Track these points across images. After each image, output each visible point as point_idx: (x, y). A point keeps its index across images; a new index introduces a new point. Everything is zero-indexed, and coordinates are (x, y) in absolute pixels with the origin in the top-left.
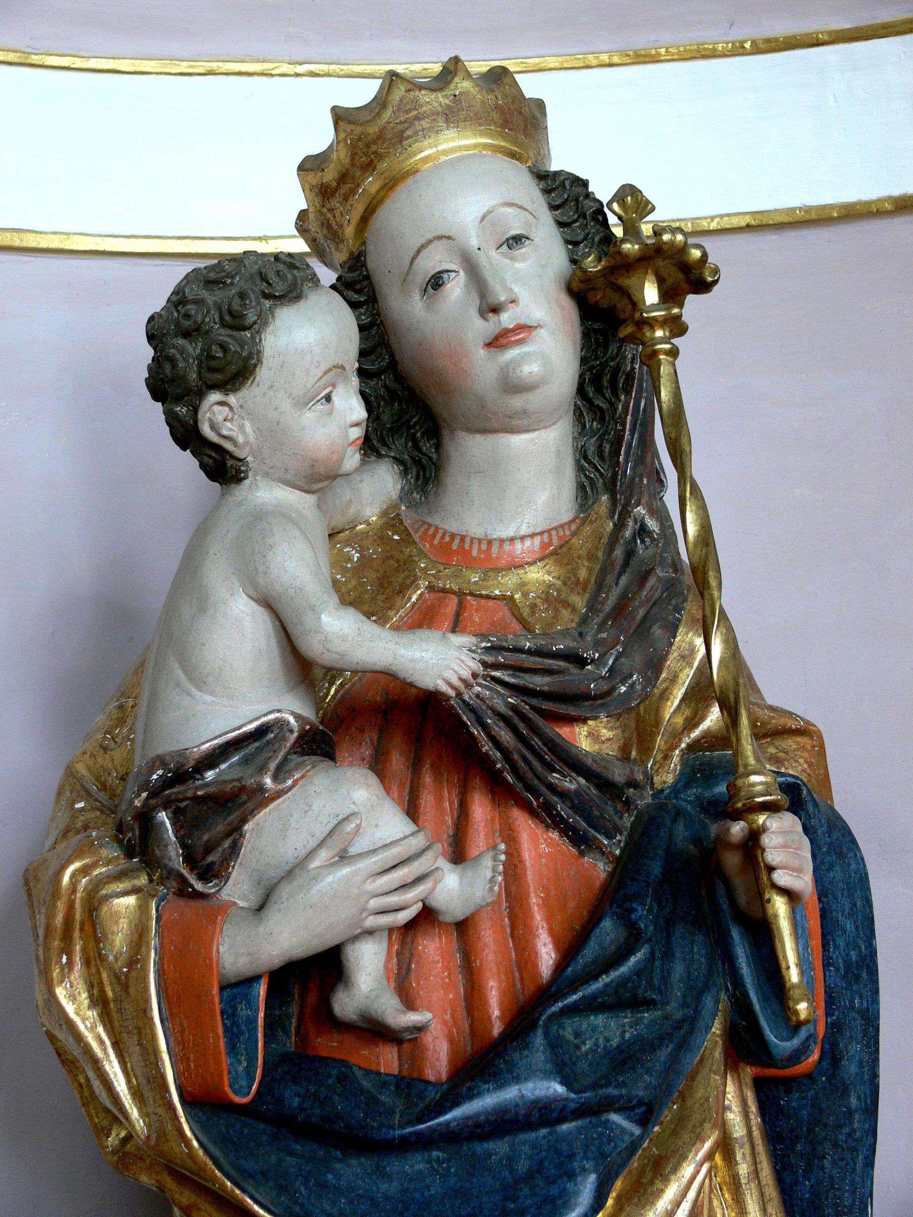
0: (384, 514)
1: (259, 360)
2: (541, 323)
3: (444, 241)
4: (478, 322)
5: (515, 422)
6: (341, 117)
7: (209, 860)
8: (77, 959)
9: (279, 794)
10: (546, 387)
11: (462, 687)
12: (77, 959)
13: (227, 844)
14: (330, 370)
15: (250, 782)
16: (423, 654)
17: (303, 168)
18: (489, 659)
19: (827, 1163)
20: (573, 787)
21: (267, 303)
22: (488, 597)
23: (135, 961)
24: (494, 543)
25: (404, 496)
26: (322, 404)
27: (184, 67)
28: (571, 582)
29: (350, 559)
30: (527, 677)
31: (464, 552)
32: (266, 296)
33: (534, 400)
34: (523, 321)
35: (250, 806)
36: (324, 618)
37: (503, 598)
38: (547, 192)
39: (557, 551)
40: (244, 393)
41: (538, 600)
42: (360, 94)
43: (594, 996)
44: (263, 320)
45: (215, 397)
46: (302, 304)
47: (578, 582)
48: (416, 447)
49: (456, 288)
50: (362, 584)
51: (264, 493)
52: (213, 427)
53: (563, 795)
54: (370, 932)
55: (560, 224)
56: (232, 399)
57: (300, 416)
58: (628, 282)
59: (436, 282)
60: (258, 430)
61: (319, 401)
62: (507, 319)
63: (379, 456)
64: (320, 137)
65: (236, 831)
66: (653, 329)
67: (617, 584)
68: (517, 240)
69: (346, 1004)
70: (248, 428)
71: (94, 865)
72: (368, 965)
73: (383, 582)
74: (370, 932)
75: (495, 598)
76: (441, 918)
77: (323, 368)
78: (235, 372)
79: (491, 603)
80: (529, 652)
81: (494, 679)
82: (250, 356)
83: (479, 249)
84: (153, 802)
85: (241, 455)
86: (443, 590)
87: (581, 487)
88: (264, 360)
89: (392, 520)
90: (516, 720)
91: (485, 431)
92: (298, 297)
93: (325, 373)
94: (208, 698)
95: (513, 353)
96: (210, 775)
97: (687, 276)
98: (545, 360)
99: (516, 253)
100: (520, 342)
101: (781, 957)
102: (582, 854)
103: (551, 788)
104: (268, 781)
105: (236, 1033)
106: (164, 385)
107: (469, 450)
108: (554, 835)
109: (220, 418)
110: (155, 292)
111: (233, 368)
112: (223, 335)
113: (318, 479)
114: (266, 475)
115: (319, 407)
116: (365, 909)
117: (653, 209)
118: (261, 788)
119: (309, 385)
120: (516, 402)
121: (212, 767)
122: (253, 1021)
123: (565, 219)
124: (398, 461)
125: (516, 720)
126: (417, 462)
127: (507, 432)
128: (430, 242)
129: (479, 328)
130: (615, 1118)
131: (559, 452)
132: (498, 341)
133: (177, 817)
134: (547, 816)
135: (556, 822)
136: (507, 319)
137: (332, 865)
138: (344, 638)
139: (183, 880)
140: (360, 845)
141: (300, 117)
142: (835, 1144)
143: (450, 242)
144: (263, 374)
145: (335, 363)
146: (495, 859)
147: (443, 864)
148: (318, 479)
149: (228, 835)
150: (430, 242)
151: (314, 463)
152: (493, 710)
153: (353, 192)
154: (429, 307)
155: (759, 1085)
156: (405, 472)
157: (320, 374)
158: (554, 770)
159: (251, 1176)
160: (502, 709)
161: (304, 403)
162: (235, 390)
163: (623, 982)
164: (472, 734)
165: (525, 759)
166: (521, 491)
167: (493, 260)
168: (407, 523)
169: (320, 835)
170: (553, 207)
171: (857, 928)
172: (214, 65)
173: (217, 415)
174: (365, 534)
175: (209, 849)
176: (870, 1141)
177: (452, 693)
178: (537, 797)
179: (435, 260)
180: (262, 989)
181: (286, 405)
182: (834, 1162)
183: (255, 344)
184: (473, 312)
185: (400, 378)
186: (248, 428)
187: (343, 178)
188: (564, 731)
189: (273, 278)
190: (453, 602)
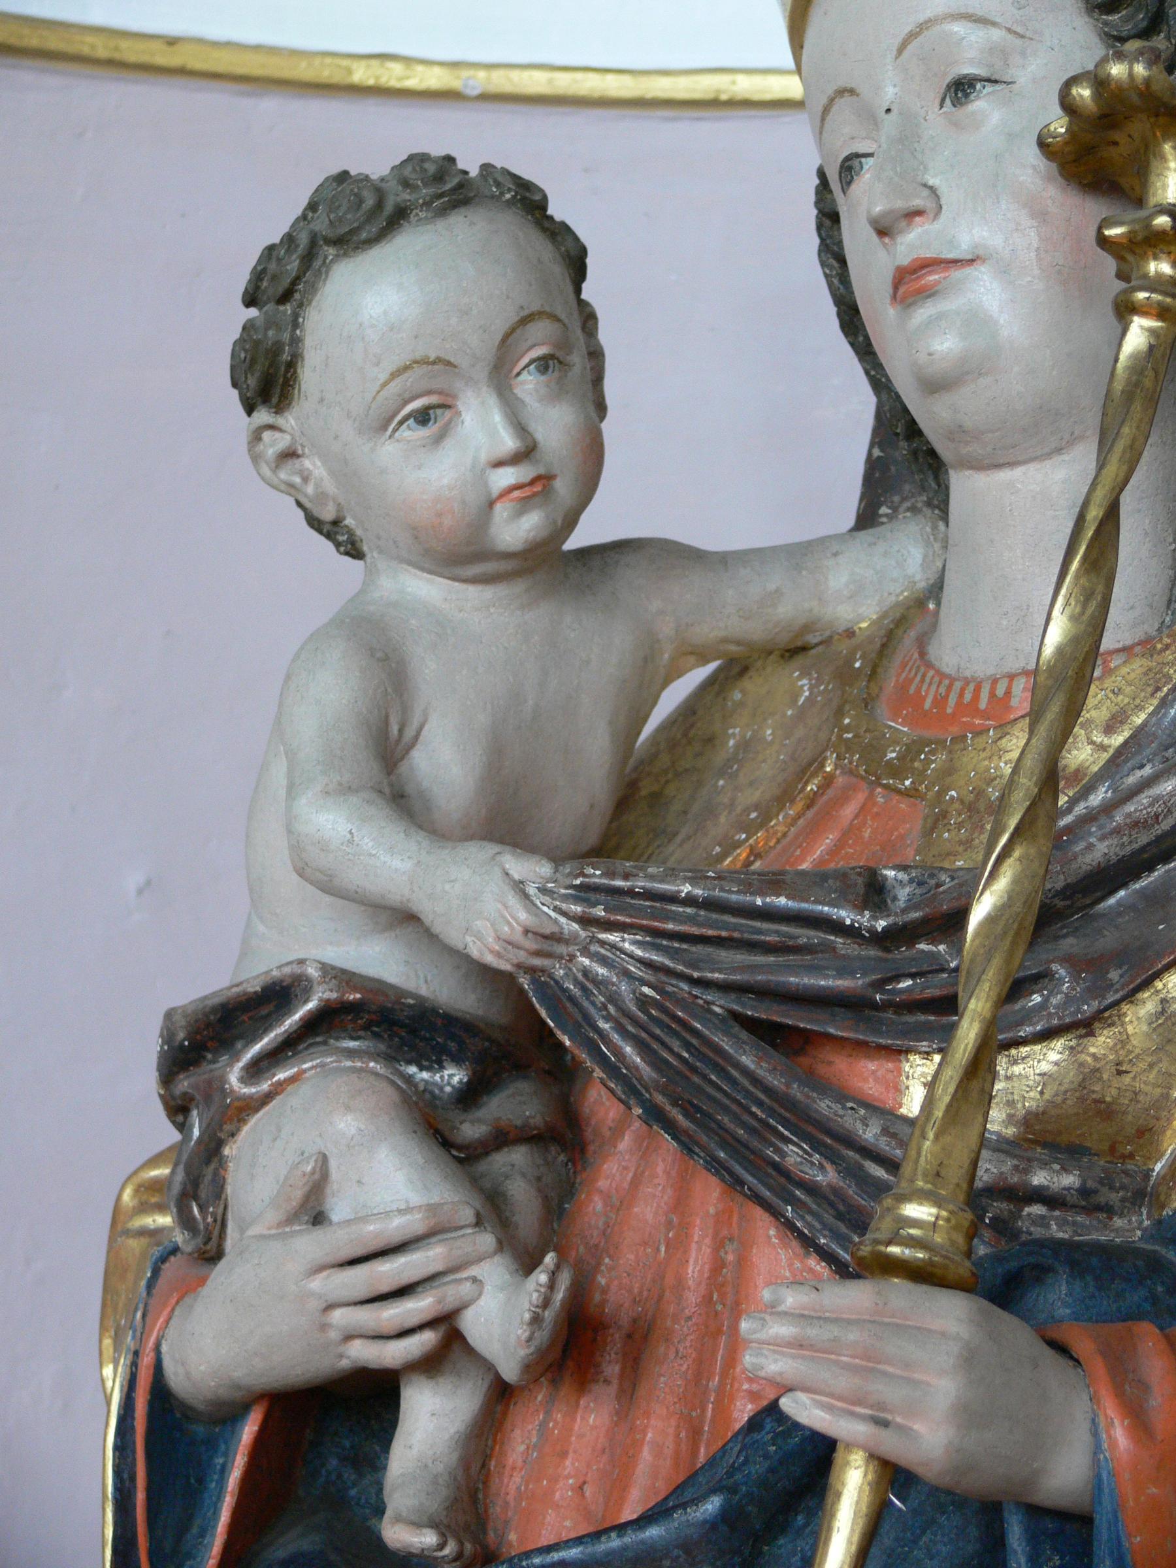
2: (981, 252)
10: (983, 381)
14: (406, 368)
16: (447, 887)
24: (984, 684)
26: (409, 428)
41: (957, 805)
57: (373, 450)
61: (401, 423)
77: (389, 366)
83: (888, 111)
88: (307, 355)
93: (394, 375)
101: (817, 1561)
119: (369, 396)
127: (971, 468)
143: (854, 98)
145: (418, 356)
157: (383, 377)
164: (561, 1045)
183: (296, 325)
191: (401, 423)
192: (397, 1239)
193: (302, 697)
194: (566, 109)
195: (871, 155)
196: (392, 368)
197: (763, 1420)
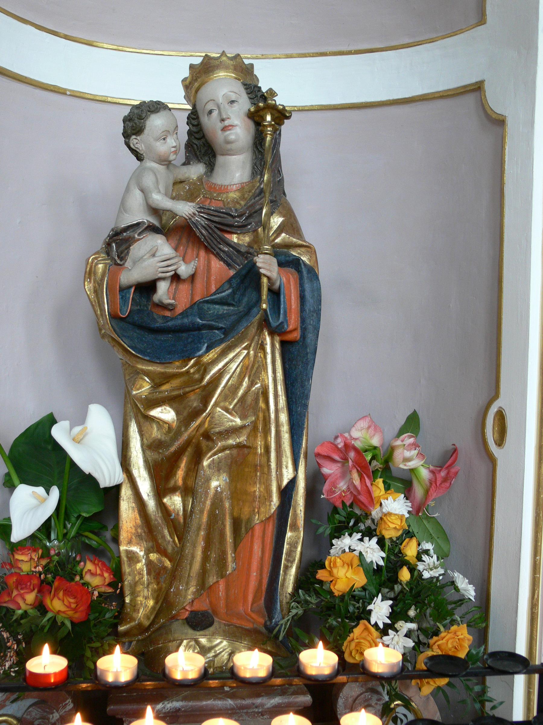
0: (198, 177)
1: (145, 128)
3: (211, 102)
4: (220, 124)
5: (229, 152)
6: (192, 67)
7: (123, 256)
8: (92, 281)
9: (139, 240)
11: (190, 217)
12: (92, 281)
13: (126, 251)
15: (132, 236)
17: (182, 81)
18: (199, 210)
19: (300, 367)
20: (227, 249)
21: (149, 113)
22: (217, 200)
23: (102, 280)
25: (206, 173)
27: (183, 54)
28: (243, 198)
29: (186, 188)
30: (213, 217)
31: (215, 188)
32: (149, 111)
33: (233, 146)
34: (231, 124)
35: (131, 241)
36: (153, 194)
37: (221, 200)
38: (246, 89)
39: (242, 189)
40: (141, 136)
42: (197, 61)
43: (214, 299)
44: (147, 117)
45: (134, 137)
46: (158, 114)
47: (244, 198)
48: (210, 160)
49: (215, 114)
50: (187, 195)
51: (150, 164)
52: (134, 145)
53: (224, 251)
54: (163, 279)
55: (250, 98)
56: (138, 138)
58: (261, 113)
59: (210, 112)
60: (145, 146)
62: (227, 123)
63: (201, 162)
64: (186, 73)
65: (128, 248)
66: (267, 127)
67: (254, 199)
68: (232, 102)
69: (156, 298)
70: (143, 146)
71: (99, 257)
72: (163, 287)
73: (192, 195)
74: (163, 279)
75: (219, 200)
76: (182, 278)
77: (162, 131)
78: (138, 131)
79: (218, 202)
80: (213, 210)
81: (202, 216)
82: (142, 126)
84: (110, 240)
85: (142, 153)
86: (206, 198)
87: (253, 173)
89: (200, 179)
90: (208, 228)
91: (223, 155)
92: (158, 112)
94: (128, 215)
95: (228, 132)
96: (125, 234)
97: (282, 115)
98: (236, 134)
99: (232, 105)
100: (230, 130)
102: (230, 269)
103: (220, 249)
104: (136, 236)
105: (124, 299)
106: (126, 135)
107: (220, 159)
108: (222, 263)
109: (135, 143)
110: (126, 111)
111: (138, 129)
112: (137, 121)
113: (166, 162)
114: (148, 159)
115: (161, 141)
116: (157, 271)
117: (277, 95)
118: (134, 237)
120: (229, 146)
121: (125, 232)
122: (129, 298)
123: (252, 97)
124: (205, 164)
125: (208, 228)
126: (210, 164)
128: (209, 101)
129: (220, 125)
130: (216, 331)
131: (244, 162)
132: (224, 129)
133: (116, 244)
134: (218, 256)
135: (222, 259)
136: (227, 123)
137: (149, 258)
138: (158, 200)
139: (115, 260)
140: (158, 254)
141: (180, 67)
142: (302, 362)
144: (146, 131)
146: (195, 262)
147: (182, 262)
148: (166, 162)
149: (126, 249)
150: (209, 101)
151: (160, 156)
152: (200, 224)
153: (192, 87)
154: (209, 119)
155: (283, 343)
156: (206, 167)
158: (221, 244)
159: (125, 337)
160: (204, 225)
161: (157, 139)
162: (139, 135)
163: (223, 298)
165: (211, 239)
166: (235, 172)
167: (225, 106)
168: (203, 180)
169: (148, 251)
170: (248, 94)
171: (314, 302)
172: (193, 54)
173: (134, 141)
174: (192, 183)
175: (122, 253)
176: (312, 362)
177: (187, 218)
178: (215, 250)
179: (210, 106)
180: (132, 290)
181: (152, 140)
182: (302, 367)
184: (218, 121)
185: (206, 141)
186: (143, 146)
187: (190, 83)
188: (227, 236)
189: (151, 107)
190: (209, 201)
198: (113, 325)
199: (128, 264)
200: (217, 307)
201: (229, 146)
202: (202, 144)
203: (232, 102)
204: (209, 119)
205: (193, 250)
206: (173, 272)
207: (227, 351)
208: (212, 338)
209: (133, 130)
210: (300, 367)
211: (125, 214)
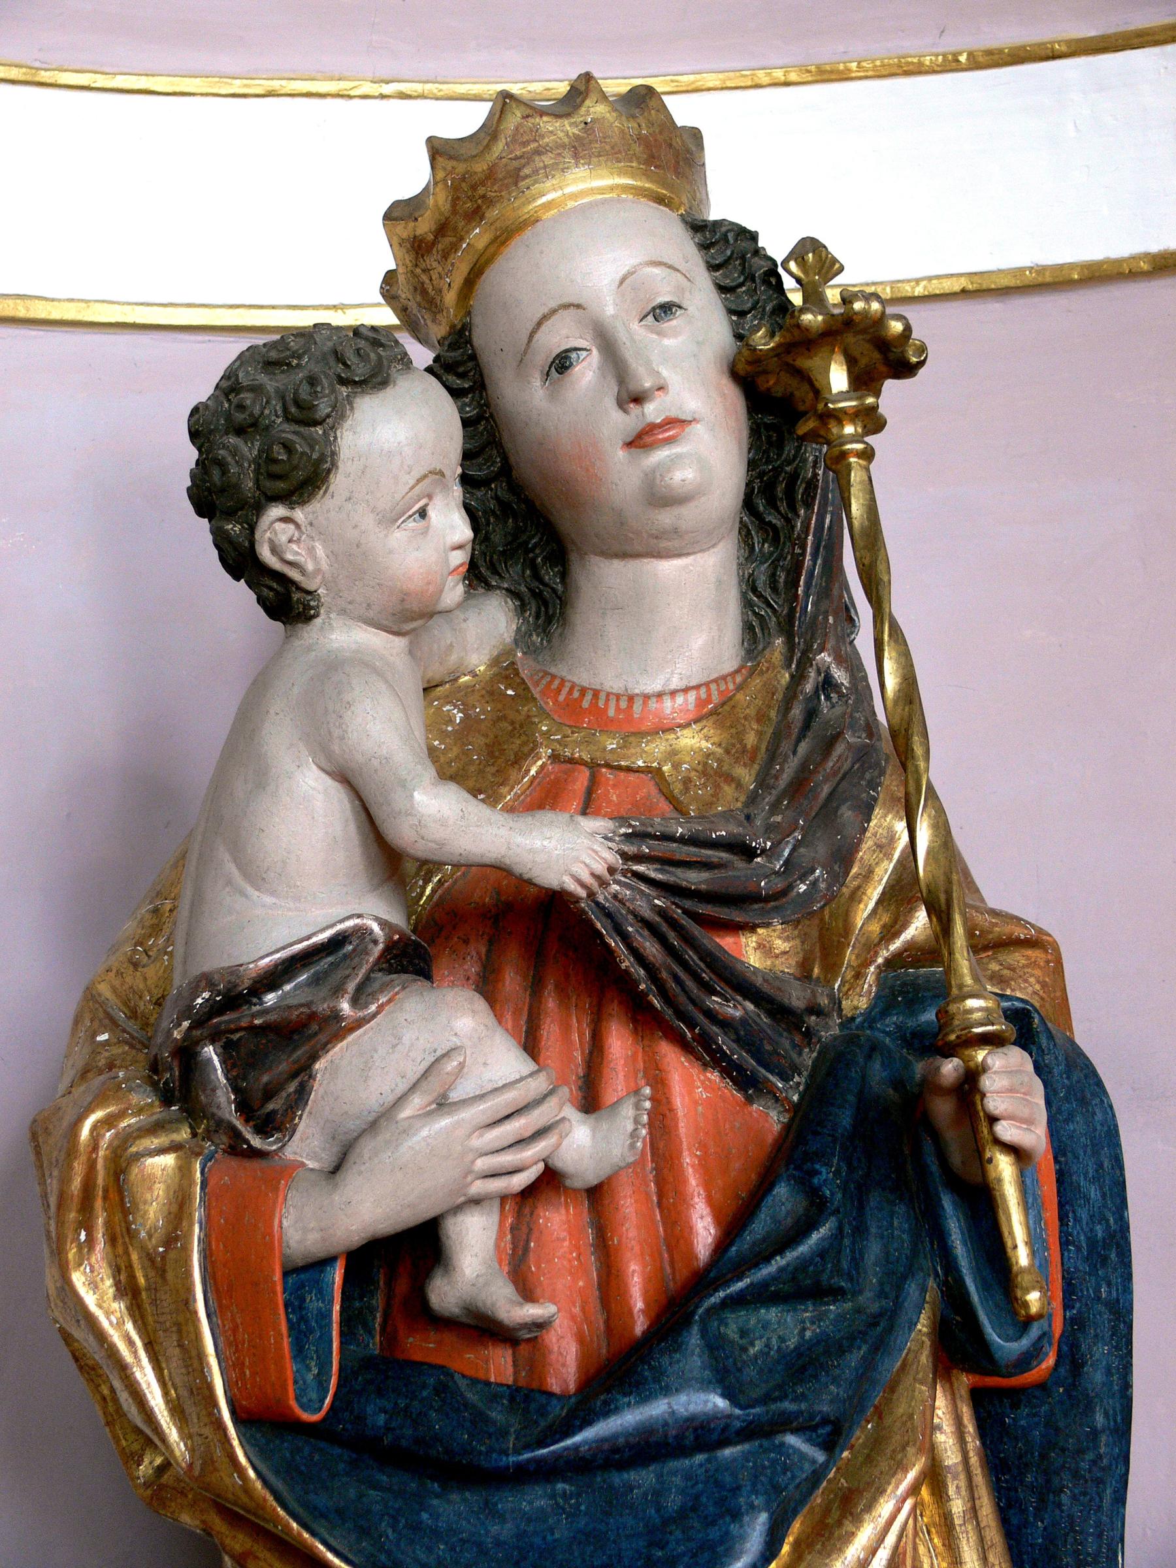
0: (495, 662)
1: (334, 464)
2: (697, 416)
3: (572, 310)
4: (616, 415)
5: (663, 544)
6: (439, 150)
7: (270, 1108)
8: (100, 1235)
9: (359, 1023)
10: (703, 499)
12: (100, 1235)
13: (292, 1087)
14: (425, 476)
15: (322, 1008)
18: (631, 849)
19: (1065, 1499)
20: (738, 1014)
21: (344, 391)
22: (629, 769)
23: (174, 1238)
25: (521, 638)
26: (414, 520)
27: (237, 86)
28: (735, 750)
29: (451, 721)
30: (679, 872)
32: (343, 382)
34: (673, 413)
35: (322, 1038)
36: (416, 794)
37: (648, 770)
38: (704, 247)
39: (717, 710)
40: (315, 506)
42: (463, 121)
44: (339, 413)
45: (277, 511)
47: (744, 750)
48: (536, 576)
49: (587, 371)
50: (466, 753)
51: (339, 635)
52: (274, 550)
53: (725, 1024)
54: (476, 1202)
55: (722, 289)
56: (299, 514)
57: (386, 536)
59: (562, 363)
60: (332, 555)
61: (410, 516)
62: (653, 411)
63: (489, 587)
65: (304, 1070)
66: (840, 423)
67: (794, 753)
68: (666, 310)
69: (445, 1294)
70: (320, 551)
71: (121, 1115)
72: (475, 1243)
73: (493, 751)
74: (476, 1202)
75: (638, 770)
76: (568, 1183)
77: (416, 474)
79: (632, 777)
80: (682, 840)
81: (636, 875)
82: (322, 459)
84: (197, 1033)
85: (311, 588)
86: (571, 761)
87: (748, 628)
88: (340, 464)
89: (504, 670)
90: (665, 928)
91: (624, 555)
92: (384, 383)
93: (419, 481)
94: (269, 900)
95: (660, 455)
96: (270, 998)
98: (702, 464)
99: (665, 325)
100: (669, 441)
102: (749, 1100)
103: (710, 1015)
104: (345, 1007)
105: (305, 1331)
106: (211, 496)
107: (604, 579)
108: (714, 1076)
109: (284, 539)
110: (200, 375)
111: (301, 475)
112: (287, 431)
113: (410, 617)
114: (343, 612)
115: (411, 524)
117: (841, 269)
118: (336, 1016)
119: (398, 497)
120: (665, 518)
121: (273, 987)
122: (326, 1315)
123: (727, 282)
124: (513, 594)
125: (665, 928)
126: (537, 595)
127: (654, 557)
128: (554, 312)
129: (617, 423)
130: (792, 1440)
132: (642, 440)
133: (228, 1053)
134: (705, 1052)
135: (716, 1059)
136: (653, 411)
137: (427, 1115)
138: (443, 822)
141: (388, 152)
142: (1076, 1474)
144: (339, 482)
145: (431, 468)
146: (637, 1106)
148: (410, 617)
150: (554, 312)
151: (404, 596)
153: (455, 247)
154: (553, 396)
155: (978, 1397)
156: (522, 608)
157: (412, 482)
158: (714, 992)
159: (323, 1516)
160: (647, 913)
161: (392, 519)
162: (303, 503)
163: (803, 1265)
165: (676, 978)
166: (671, 632)
167: (635, 335)
168: (525, 673)
169: (412, 1077)
170: (712, 267)
172: (275, 85)
173: (280, 534)
174: (469, 689)
175: (269, 1093)
176: (1121, 1469)
177: (583, 893)
178: (691, 1027)
179: (560, 335)
180: (337, 1275)
181: (368, 521)
182: (1074, 1497)
183: (328, 443)
184: (610, 403)
186: (320, 551)
187: (442, 229)
188: (727, 942)
190: (583, 775)
191: (410, 516)
192: (507, 1122)
193: (390, 720)
194: (948, 300)
195: (585, 349)
196: (418, 476)
197: (84, 1216)
198: (253, 1459)
199: (306, 1144)
200: (771, 1314)
201: (665, 518)
202: (492, 504)
203: (666, 310)
204: (553, 396)
205: (566, 1028)
206: (541, 1166)
207: (839, 1523)
208: (782, 1480)
209: (273, 477)
210: (1065, 1499)
211: (254, 894)
